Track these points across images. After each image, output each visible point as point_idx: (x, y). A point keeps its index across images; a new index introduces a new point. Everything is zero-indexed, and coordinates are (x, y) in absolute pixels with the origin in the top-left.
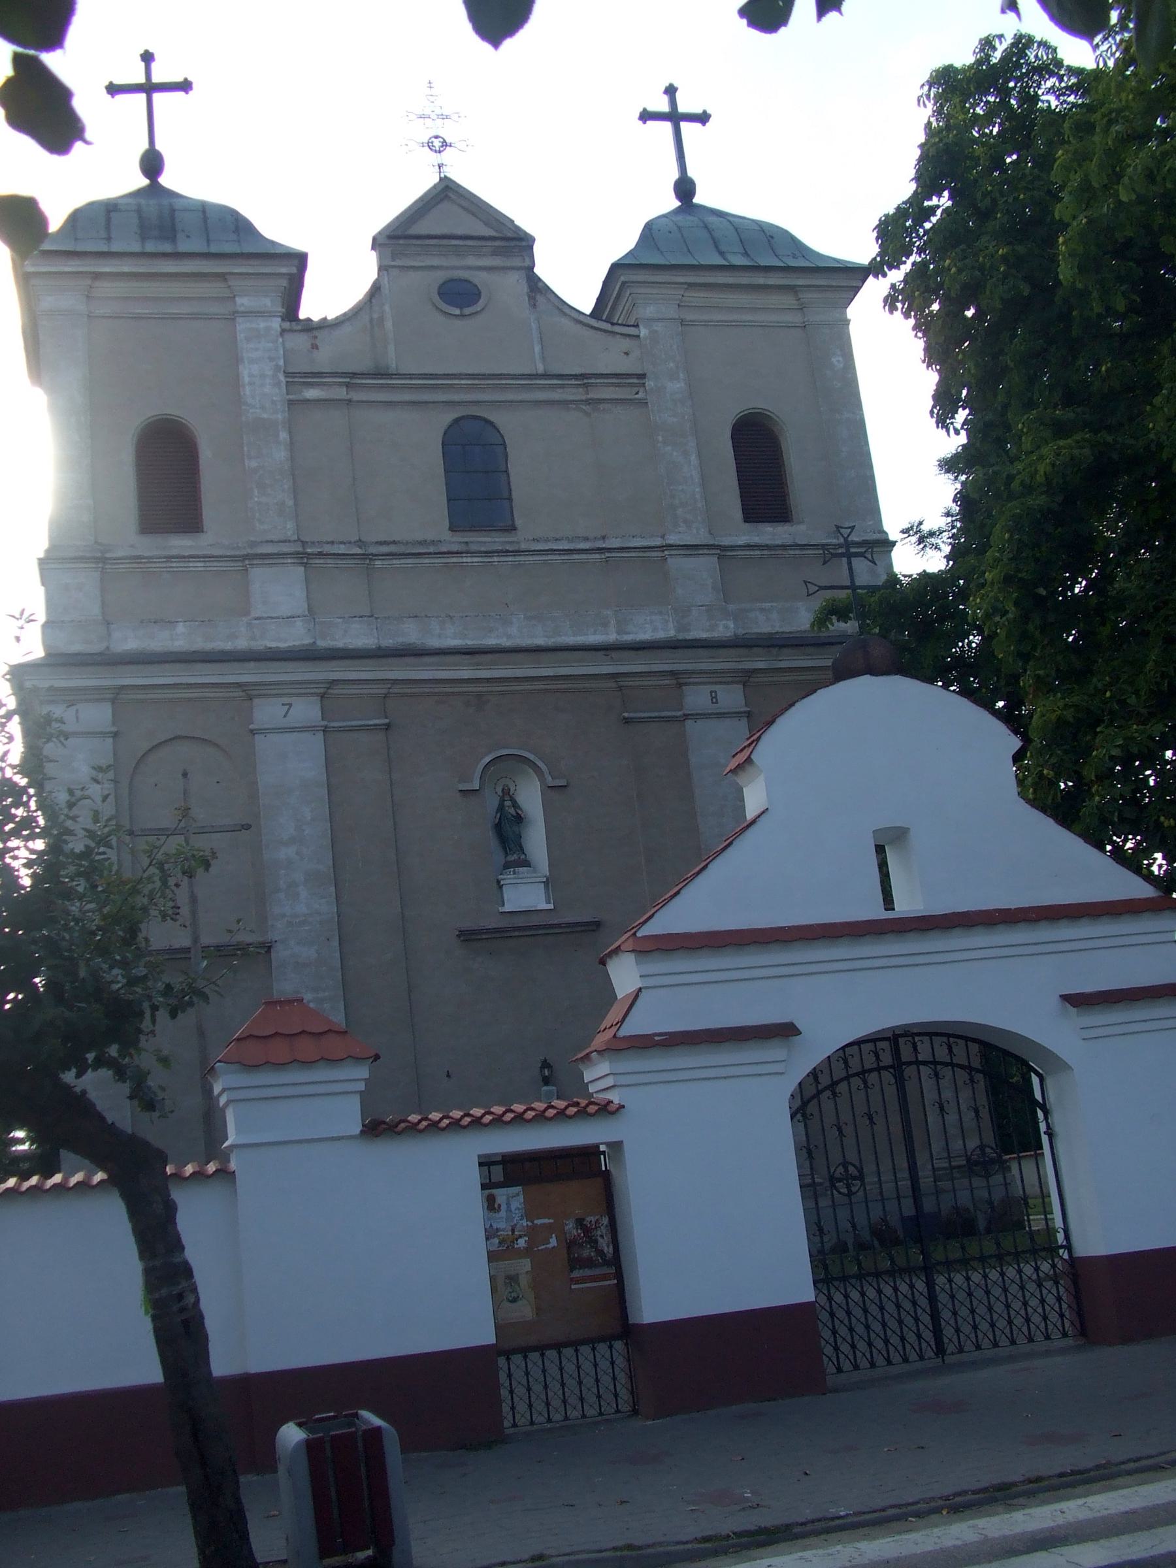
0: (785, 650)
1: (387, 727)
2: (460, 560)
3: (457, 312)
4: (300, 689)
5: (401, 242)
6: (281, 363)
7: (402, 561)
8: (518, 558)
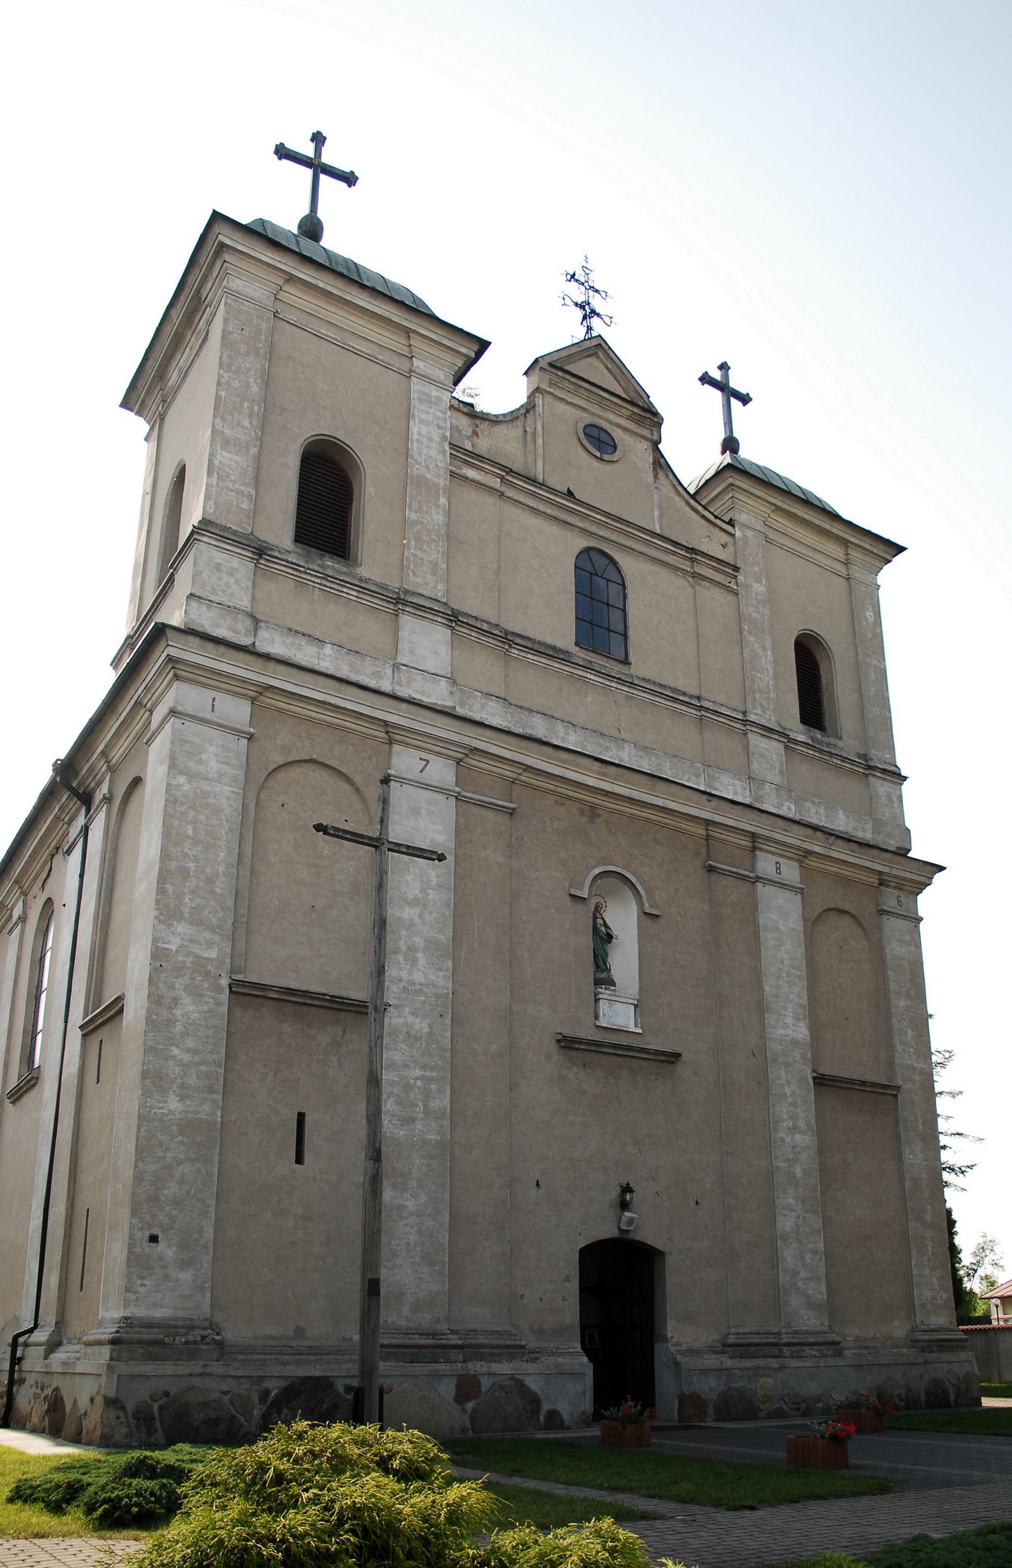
0: (839, 842)
1: (512, 813)
2: (585, 674)
3: (598, 454)
4: (439, 746)
5: (560, 373)
6: (448, 434)
7: (536, 658)
8: (632, 691)
